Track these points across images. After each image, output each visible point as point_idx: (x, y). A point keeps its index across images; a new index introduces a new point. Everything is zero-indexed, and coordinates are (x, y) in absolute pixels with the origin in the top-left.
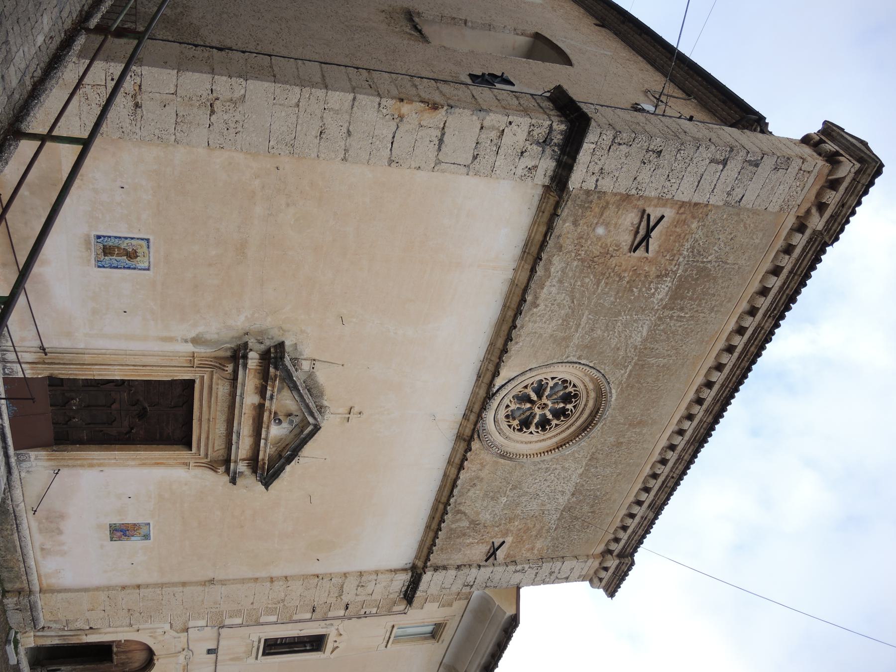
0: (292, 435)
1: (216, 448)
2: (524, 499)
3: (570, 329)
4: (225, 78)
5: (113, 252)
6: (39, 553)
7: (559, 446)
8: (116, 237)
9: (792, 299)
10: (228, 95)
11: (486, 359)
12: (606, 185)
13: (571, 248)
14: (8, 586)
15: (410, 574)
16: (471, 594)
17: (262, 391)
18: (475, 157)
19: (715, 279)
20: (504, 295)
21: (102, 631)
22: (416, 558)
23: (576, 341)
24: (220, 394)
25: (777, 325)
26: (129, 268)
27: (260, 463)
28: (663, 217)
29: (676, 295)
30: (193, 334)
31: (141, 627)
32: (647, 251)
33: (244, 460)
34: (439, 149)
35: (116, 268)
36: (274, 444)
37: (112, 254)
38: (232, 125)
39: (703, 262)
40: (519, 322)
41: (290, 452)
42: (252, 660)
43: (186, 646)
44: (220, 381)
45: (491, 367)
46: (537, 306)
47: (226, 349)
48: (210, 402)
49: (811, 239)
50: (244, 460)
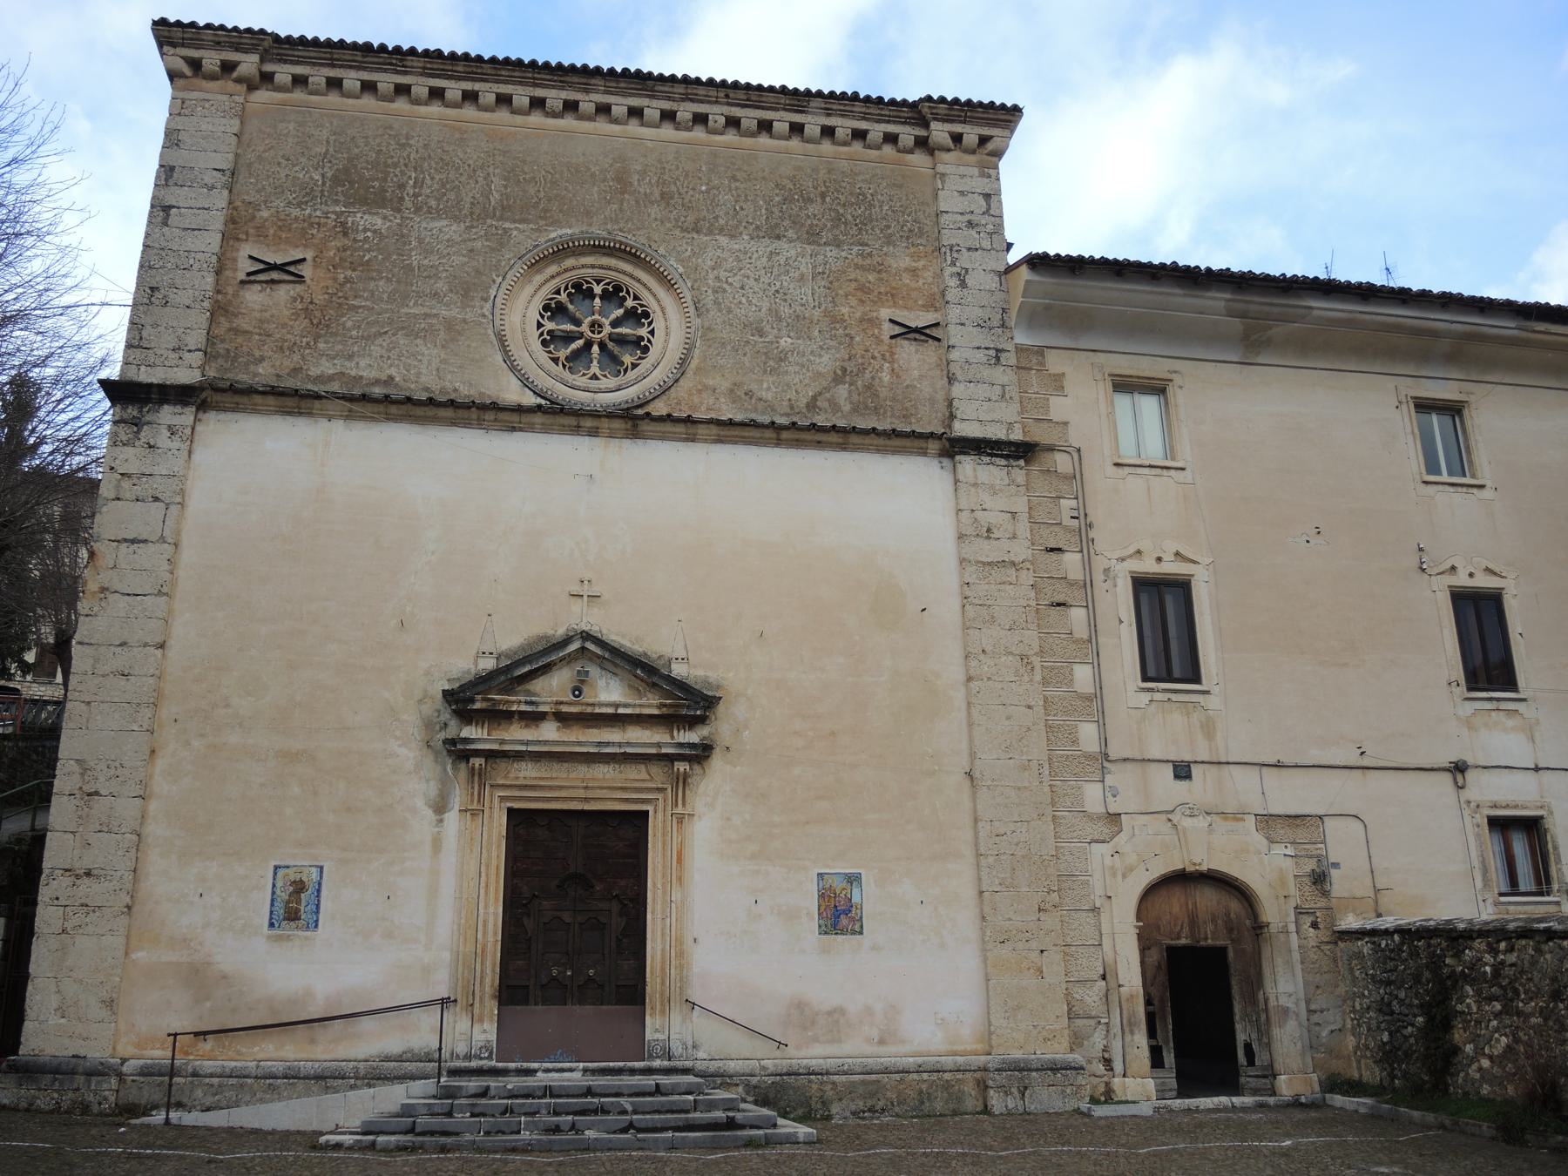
0: (618, 671)
1: (644, 776)
2: (785, 311)
3: (431, 325)
4: (56, 782)
5: (295, 907)
6: (891, 1049)
7: (669, 284)
8: (272, 905)
9: (367, 48)
10: (76, 777)
11: (480, 425)
12: (196, 338)
13: (296, 357)
14: (971, 1103)
15: (958, 458)
16: (1020, 349)
17: (534, 718)
18: (156, 499)
19: (350, 160)
20: (373, 424)
21: (1109, 957)
22: (925, 454)
23: (455, 312)
24: (534, 774)
25: (412, 51)
26: (319, 891)
27: (671, 711)
28: (251, 257)
29: (376, 200)
30: (429, 813)
31: (1099, 891)
32: (304, 260)
33: (672, 737)
34: (145, 541)
35: (318, 906)
36: (640, 695)
37: (297, 911)
38: (112, 772)
39: (324, 184)
40: (443, 399)
41: (643, 670)
42: (1213, 702)
43: (1164, 817)
44: (511, 776)
45: (490, 416)
46: (391, 378)
47: (455, 769)
48: (551, 788)
49: (280, 61)
50: (672, 737)
